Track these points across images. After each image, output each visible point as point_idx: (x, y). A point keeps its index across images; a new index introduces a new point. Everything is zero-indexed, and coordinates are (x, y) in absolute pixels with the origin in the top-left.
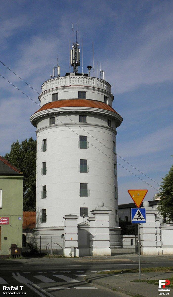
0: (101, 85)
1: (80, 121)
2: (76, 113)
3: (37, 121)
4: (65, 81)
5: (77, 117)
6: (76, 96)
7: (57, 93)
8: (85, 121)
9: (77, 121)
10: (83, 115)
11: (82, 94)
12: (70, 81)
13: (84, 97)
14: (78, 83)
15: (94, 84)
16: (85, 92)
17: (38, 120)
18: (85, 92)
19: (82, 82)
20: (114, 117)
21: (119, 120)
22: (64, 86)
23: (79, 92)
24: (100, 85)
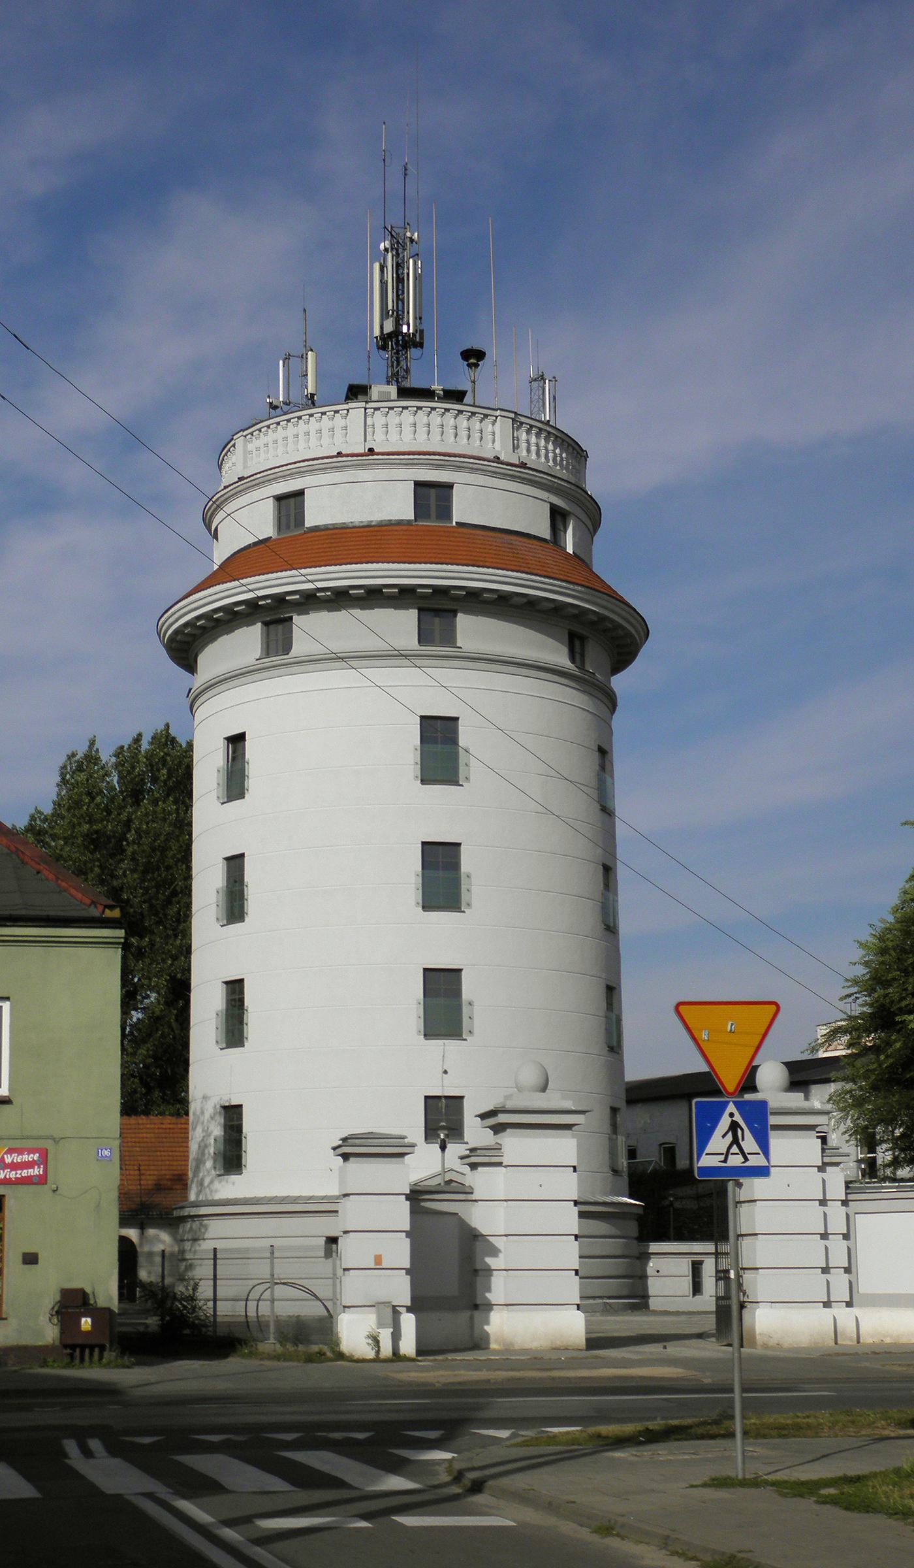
2: (404, 596)
4: (342, 428)
6: (401, 506)
7: (300, 493)
11: (432, 497)
12: (369, 430)
13: (445, 511)
14: (439, 437)
15: (498, 445)
16: (449, 486)
18: (449, 486)
19: (463, 434)
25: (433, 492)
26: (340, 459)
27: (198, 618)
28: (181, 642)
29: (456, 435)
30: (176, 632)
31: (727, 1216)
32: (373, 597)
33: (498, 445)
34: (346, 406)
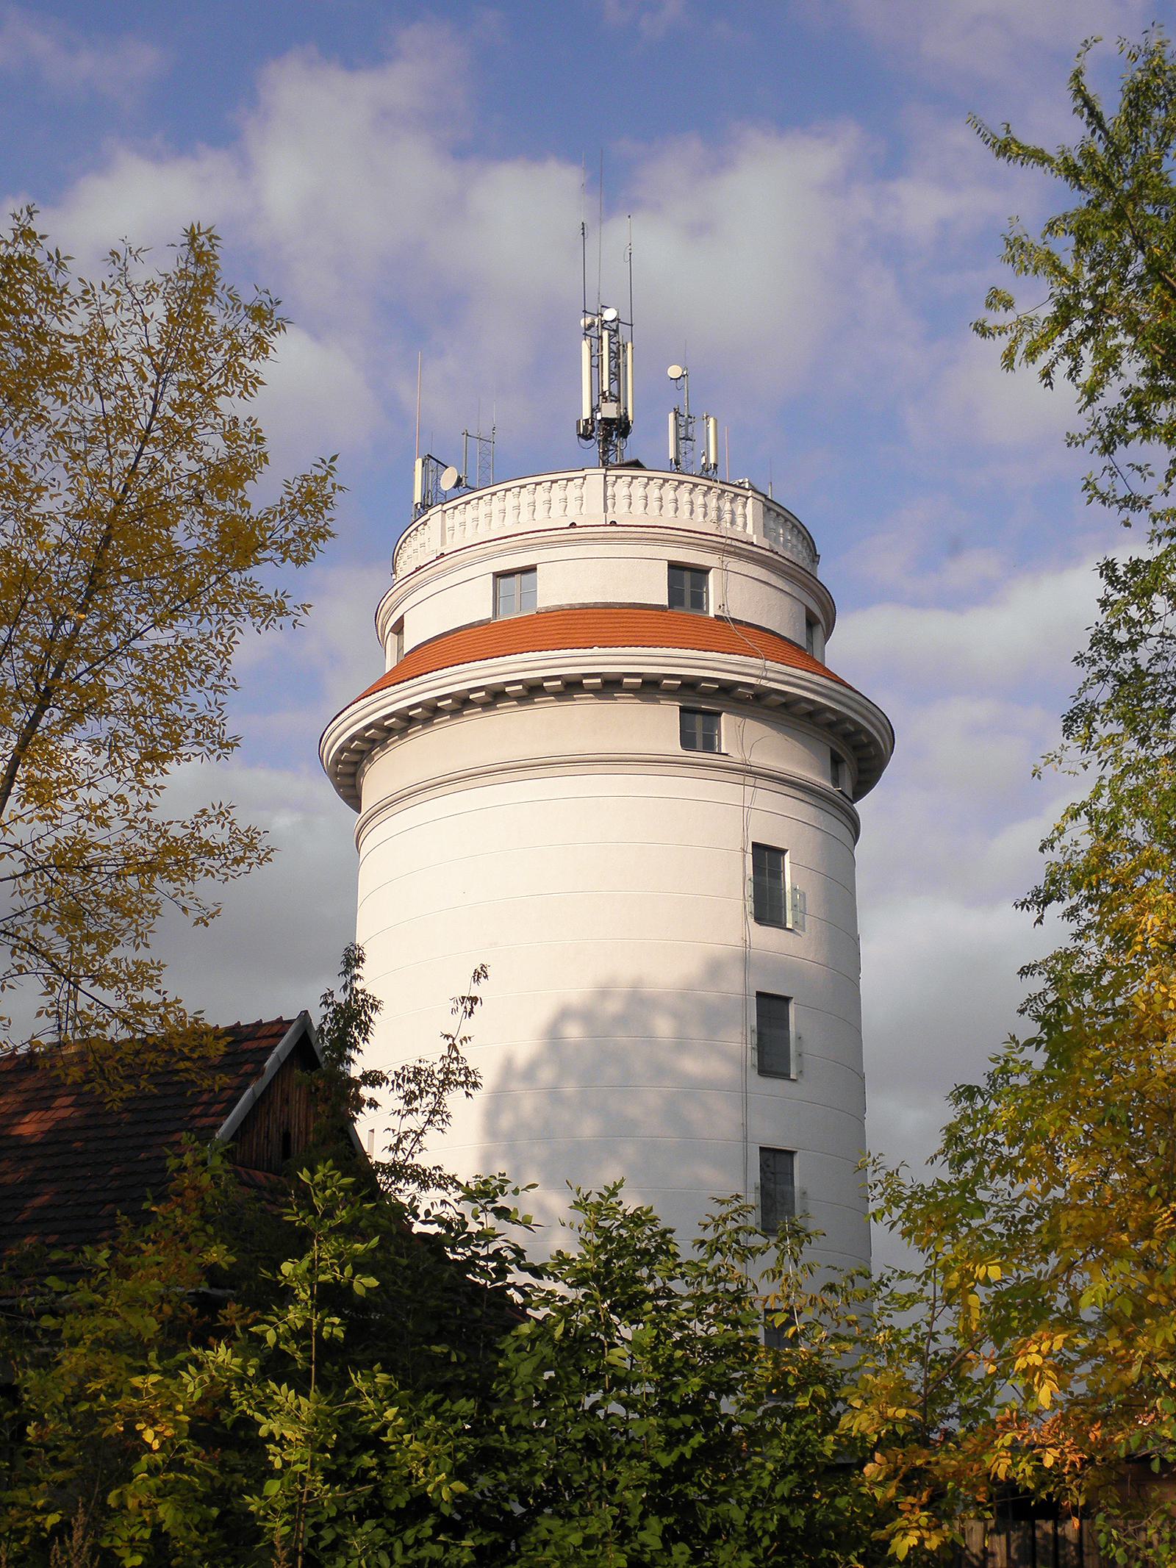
0: (727, 517)
1: (687, 741)
2: (650, 688)
3: (373, 742)
4: (584, 495)
5: (666, 716)
6: (653, 588)
7: (531, 569)
8: (709, 745)
9: (673, 746)
10: (701, 707)
11: (688, 581)
12: (609, 502)
13: (698, 601)
14: (672, 513)
15: (750, 530)
16: (704, 571)
17: (380, 735)
18: (704, 571)
19: (654, 505)
20: (844, 719)
21: (873, 742)
22: (573, 525)
23: (674, 567)
24: (733, 522)
25: (687, 575)
26: (572, 530)
27: (367, 728)
28: (344, 763)
29: (677, 509)
30: (342, 750)
31: (792, 1174)
32: (610, 686)
33: (750, 530)
34: (582, 474)
